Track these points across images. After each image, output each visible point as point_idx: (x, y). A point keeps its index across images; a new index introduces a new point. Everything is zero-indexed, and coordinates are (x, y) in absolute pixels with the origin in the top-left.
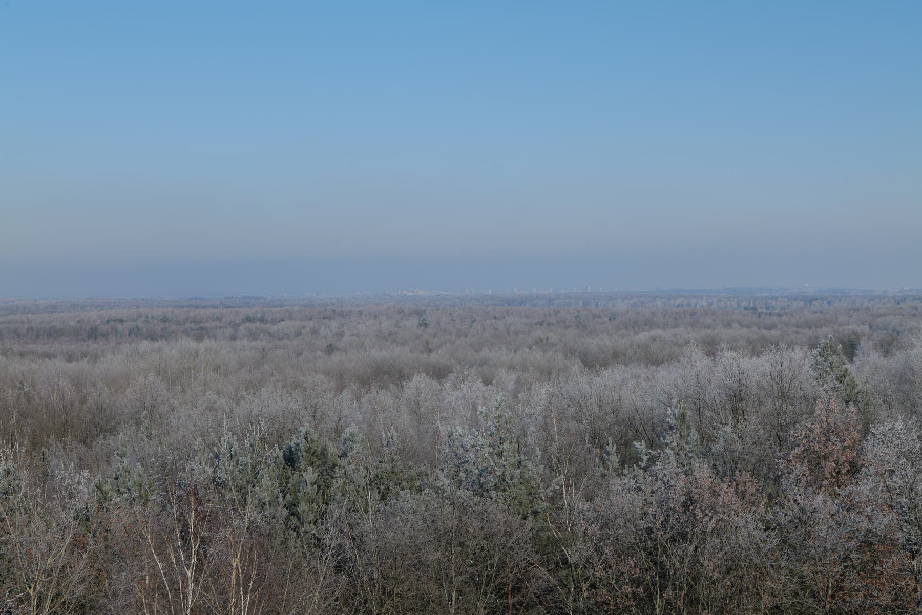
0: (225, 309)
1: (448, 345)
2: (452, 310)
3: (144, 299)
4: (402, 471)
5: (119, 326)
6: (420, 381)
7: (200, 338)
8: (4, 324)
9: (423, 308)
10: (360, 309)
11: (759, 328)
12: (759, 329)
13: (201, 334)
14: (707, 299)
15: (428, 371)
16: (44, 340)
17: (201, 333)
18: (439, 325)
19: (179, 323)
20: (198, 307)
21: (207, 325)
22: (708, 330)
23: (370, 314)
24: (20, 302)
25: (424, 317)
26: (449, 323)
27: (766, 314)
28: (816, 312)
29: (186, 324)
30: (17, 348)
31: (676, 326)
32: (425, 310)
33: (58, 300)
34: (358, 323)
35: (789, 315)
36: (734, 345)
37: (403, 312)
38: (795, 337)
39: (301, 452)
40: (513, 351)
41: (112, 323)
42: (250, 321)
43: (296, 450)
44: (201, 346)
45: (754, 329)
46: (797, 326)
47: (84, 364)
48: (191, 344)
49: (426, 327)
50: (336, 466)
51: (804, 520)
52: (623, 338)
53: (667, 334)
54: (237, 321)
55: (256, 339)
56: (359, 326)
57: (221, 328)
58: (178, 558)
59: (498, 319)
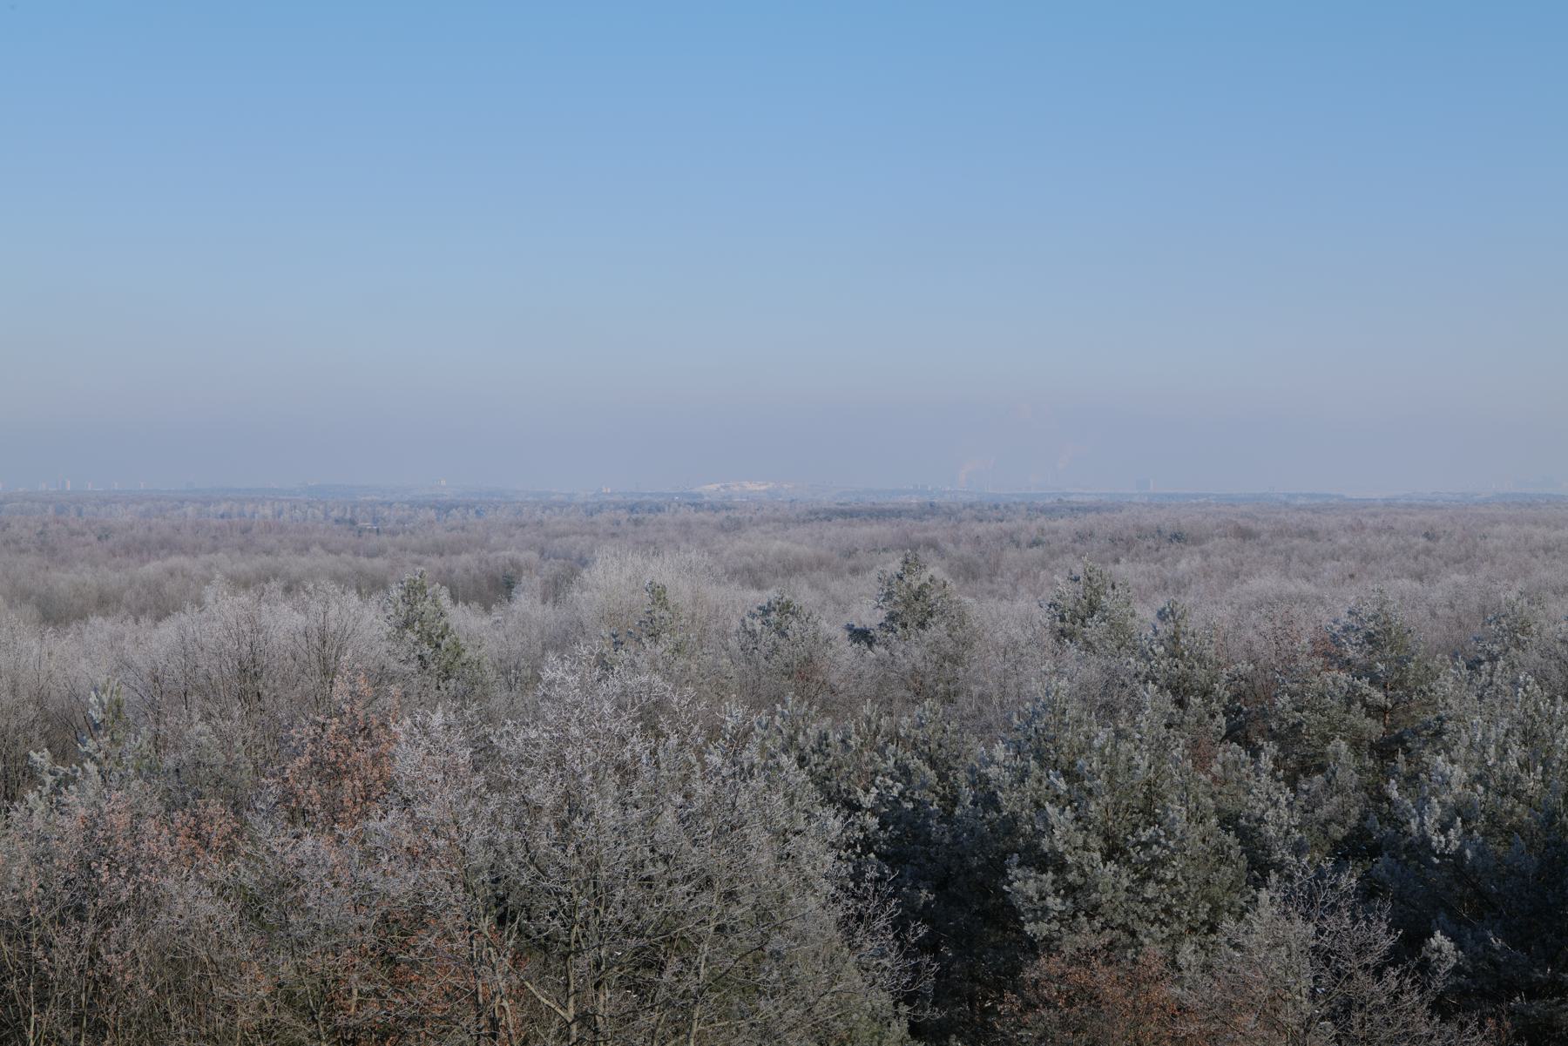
11: (356, 554)
14: (273, 504)
27: (370, 531)
31: (215, 549)
35: (408, 533)
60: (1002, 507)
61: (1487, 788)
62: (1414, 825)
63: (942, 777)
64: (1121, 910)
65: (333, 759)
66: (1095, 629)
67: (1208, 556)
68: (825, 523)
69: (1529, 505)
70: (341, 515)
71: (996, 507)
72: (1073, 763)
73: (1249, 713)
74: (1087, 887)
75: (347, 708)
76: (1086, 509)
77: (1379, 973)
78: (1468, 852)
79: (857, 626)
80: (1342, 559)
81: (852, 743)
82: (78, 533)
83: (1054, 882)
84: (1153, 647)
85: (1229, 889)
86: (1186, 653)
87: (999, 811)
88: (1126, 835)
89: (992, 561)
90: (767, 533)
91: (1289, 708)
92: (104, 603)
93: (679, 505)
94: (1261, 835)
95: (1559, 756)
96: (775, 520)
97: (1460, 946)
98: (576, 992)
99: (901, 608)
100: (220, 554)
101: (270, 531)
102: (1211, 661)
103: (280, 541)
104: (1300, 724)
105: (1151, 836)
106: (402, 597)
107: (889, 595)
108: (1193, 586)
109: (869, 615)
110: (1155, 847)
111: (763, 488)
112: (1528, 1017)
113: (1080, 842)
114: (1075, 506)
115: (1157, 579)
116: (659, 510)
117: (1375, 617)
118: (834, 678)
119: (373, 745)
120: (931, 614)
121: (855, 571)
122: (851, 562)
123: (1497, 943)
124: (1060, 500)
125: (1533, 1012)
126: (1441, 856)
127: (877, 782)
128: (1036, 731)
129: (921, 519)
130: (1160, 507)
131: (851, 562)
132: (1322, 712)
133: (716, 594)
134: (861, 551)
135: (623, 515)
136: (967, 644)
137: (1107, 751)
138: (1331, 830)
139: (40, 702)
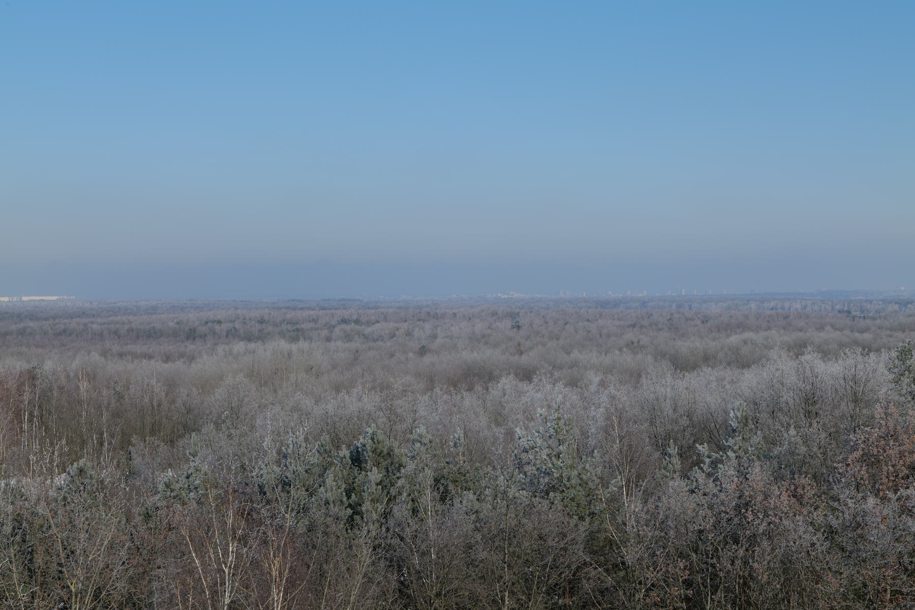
0: (321, 311)
1: (540, 347)
2: (546, 312)
3: (242, 301)
4: (468, 472)
5: (217, 327)
6: (507, 382)
7: (295, 339)
8: (106, 325)
9: (518, 310)
10: (454, 311)
11: (852, 331)
12: (852, 332)
13: (297, 336)
14: (801, 302)
15: (518, 373)
16: (143, 340)
17: (296, 334)
18: (532, 327)
19: (275, 325)
20: (295, 309)
21: (303, 326)
22: (800, 333)
23: (464, 316)
24: (121, 303)
25: (518, 319)
26: (541, 325)
27: (860, 317)
28: (910, 316)
29: (283, 325)
30: (116, 348)
31: (769, 328)
32: (519, 313)
33: (159, 302)
34: (452, 325)
35: (883, 318)
36: (826, 348)
37: (496, 314)
38: (888, 340)
39: (367, 452)
40: (603, 353)
41: (210, 325)
42: (346, 322)
43: (363, 451)
44: (294, 347)
45: (847, 332)
46: (891, 330)
47: (179, 365)
48: (284, 345)
49: (519, 329)
50: (402, 466)
51: (858, 525)
52: (714, 341)
53: (758, 337)
54: (333, 323)
55: (351, 341)
56: (453, 328)
57: (317, 329)
58: (216, 553)
59: (591, 322)
75: (883, 423)
92: (708, 359)
101: (800, 318)
103: (807, 324)
106: (897, 356)
119: (899, 445)
139: (120, 397)
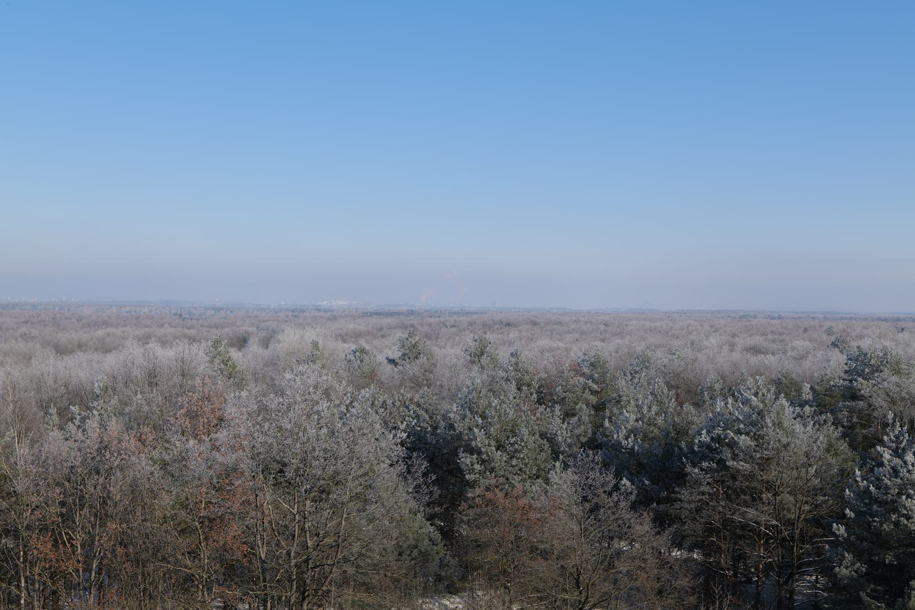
11: (183, 328)
27: (188, 319)
31: (125, 325)
60: (439, 312)
61: (643, 422)
62: (615, 436)
63: (431, 417)
64: (503, 470)
65: (195, 410)
66: (484, 360)
67: (521, 332)
68: (370, 317)
69: (643, 313)
70: (176, 312)
71: (437, 312)
72: (484, 412)
73: (545, 393)
74: (490, 461)
76: (472, 313)
77: (610, 494)
78: (636, 448)
79: (390, 358)
80: (573, 333)
81: (397, 404)
82: (69, 318)
83: (477, 459)
84: (509, 367)
85: (544, 461)
86: (521, 370)
87: (455, 431)
88: (505, 440)
89: (436, 333)
90: (347, 321)
91: (561, 391)
93: (312, 310)
94: (555, 440)
95: (671, 410)
96: (350, 316)
97: (633, 484)
98: (298, 502)
99: (407, 351)
100: (128, 327)
102: (531, 373)
104: (565, 398)
105: (515, 441)
107: (403, 346)
108: (516, 344)
109: (395, 354)
110: (516, 445)
111: (345, 303)
112: (658, 511)
113: (487, 443)
114: (468, 312)
115: (501, 341)
116: (304, 312)
117: (594, 356)
118: (383, 379)
119: (211, 405)
120: (420, 354)
121: (383, 336)
122: (381, 333)
123: (647, 482)
124: (462, 309)
125: (661, 509)
126: (626, 449)
127: (406, 419)
128: (469, 399)
129: (407, 316)
130: (501, 312)
131: (381, 333)
132: (573, 393)
133: (331, 344)
134: (385, 329)
135: (290, 314)
136: (435, 365)
137: (498, 407)
138: (581, 439)
